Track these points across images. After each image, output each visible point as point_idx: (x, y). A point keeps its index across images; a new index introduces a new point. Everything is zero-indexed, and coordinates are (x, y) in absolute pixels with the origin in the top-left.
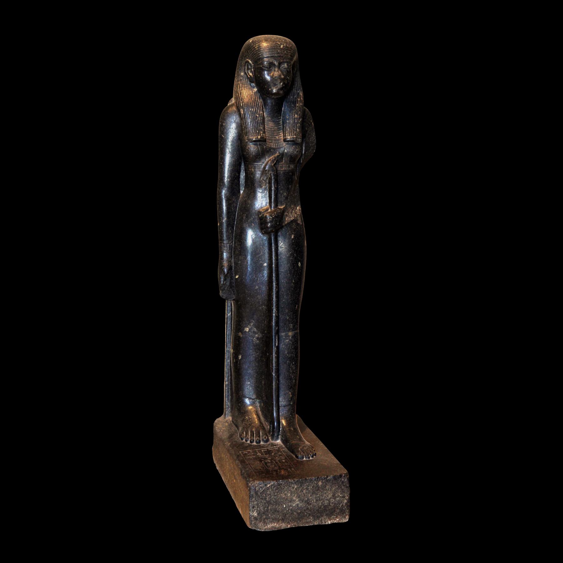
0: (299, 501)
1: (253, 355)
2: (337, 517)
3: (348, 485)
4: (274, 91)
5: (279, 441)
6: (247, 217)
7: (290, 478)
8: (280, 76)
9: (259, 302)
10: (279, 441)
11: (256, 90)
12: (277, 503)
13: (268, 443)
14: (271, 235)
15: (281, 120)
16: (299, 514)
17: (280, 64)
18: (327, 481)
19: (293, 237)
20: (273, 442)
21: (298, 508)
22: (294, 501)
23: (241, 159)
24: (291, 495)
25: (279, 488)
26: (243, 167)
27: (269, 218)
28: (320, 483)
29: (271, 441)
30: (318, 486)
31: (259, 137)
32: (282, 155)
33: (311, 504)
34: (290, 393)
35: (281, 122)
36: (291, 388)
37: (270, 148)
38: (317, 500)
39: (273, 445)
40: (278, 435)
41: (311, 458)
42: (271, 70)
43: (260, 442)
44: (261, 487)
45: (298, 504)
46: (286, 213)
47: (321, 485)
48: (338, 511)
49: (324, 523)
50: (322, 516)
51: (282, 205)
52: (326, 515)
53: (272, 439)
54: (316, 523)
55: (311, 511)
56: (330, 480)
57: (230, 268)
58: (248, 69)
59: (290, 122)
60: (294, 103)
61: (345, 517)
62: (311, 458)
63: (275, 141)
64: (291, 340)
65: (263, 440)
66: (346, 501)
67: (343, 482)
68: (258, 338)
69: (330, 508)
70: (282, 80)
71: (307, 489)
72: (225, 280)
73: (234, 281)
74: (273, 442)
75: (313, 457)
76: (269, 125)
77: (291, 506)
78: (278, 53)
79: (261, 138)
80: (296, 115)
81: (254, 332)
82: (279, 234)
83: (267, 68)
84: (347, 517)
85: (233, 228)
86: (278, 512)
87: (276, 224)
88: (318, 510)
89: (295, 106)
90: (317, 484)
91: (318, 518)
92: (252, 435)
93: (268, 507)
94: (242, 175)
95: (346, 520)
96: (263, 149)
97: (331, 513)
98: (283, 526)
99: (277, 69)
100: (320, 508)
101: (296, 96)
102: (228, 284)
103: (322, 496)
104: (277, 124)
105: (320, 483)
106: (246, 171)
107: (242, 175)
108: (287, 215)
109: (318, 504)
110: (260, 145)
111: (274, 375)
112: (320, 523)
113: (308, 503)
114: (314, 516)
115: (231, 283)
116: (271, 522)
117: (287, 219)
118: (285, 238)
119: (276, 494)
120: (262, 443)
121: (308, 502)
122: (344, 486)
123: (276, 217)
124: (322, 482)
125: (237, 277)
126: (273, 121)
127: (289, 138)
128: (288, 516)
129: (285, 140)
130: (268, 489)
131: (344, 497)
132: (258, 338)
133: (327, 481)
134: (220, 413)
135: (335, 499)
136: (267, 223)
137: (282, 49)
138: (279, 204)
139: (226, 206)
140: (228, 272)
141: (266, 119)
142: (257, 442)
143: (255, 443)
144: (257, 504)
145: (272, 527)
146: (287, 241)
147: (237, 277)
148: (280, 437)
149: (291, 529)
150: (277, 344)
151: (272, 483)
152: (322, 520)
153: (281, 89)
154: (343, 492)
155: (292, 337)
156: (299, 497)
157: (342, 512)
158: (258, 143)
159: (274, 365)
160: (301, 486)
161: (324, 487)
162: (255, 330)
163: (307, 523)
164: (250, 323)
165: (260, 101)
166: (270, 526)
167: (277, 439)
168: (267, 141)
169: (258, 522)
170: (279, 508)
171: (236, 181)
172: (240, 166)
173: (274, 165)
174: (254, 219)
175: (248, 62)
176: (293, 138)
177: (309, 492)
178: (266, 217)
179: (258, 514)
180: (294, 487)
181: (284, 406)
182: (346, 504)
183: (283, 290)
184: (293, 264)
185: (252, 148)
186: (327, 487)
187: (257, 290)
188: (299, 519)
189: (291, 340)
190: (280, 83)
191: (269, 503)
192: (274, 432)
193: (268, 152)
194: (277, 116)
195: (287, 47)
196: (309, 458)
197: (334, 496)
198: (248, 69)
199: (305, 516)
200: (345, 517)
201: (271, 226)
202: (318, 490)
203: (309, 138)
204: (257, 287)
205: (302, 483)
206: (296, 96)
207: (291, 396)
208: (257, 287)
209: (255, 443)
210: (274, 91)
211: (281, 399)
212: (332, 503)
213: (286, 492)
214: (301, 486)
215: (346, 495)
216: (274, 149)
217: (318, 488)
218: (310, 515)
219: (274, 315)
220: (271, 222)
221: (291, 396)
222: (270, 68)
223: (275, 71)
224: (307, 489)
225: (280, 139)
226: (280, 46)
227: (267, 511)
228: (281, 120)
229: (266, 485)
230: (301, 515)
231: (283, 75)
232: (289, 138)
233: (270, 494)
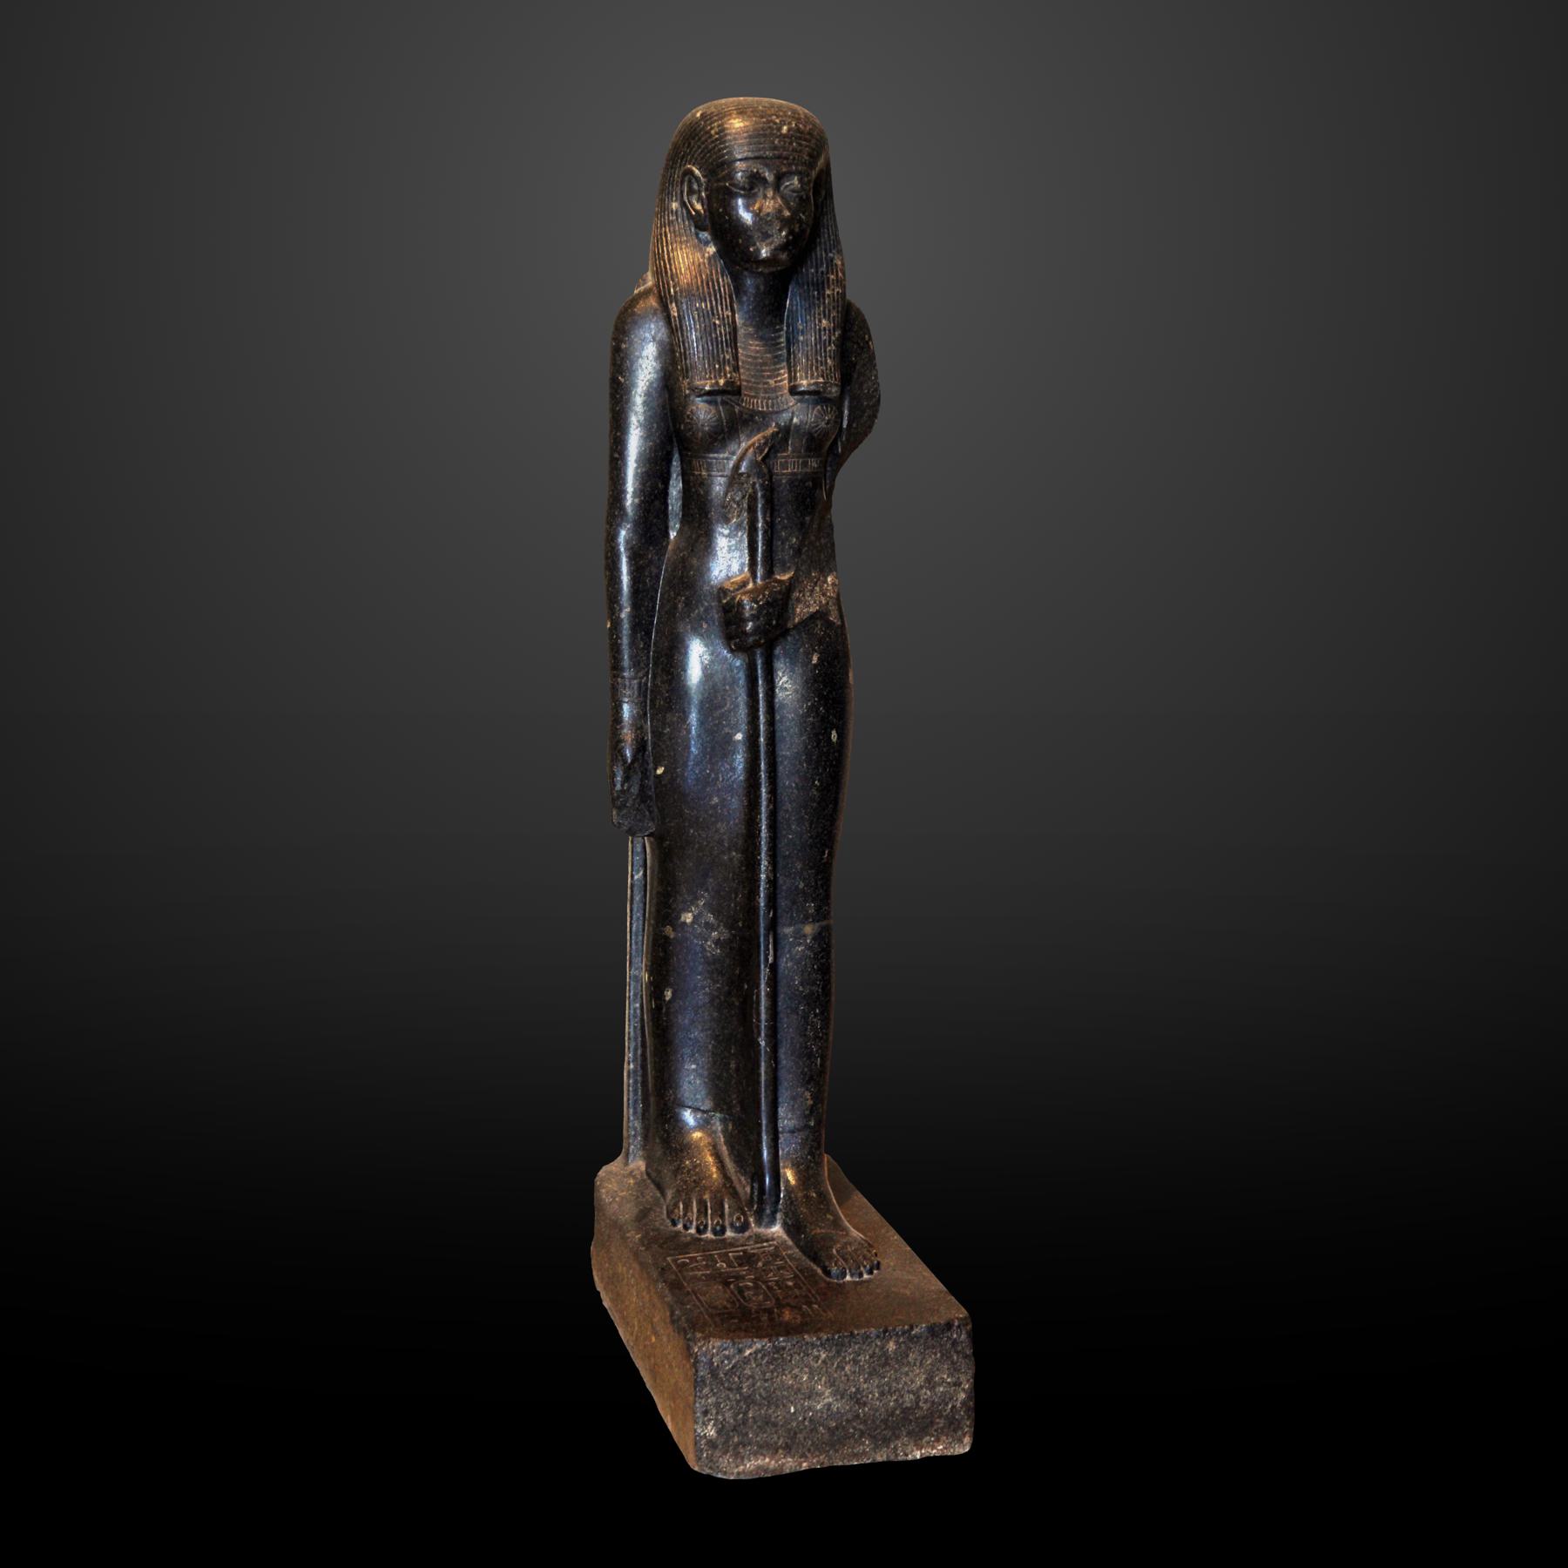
0: (833, 1394)
1: (703, 988)
2: (938, 1440)
4: (764, 253)
5: (777, 1229)
6: (688, 604)
7: (808, 1332)
8: (780, 211)
9: (721, 842)
10: (777, 1229)
11: (712, 249)
12: (771, 1400)
13: (747, 1234)
14: (754, 654)
15: (783, 333)
16: (832, 1431)
17: (779, 178)
18: (911, 1339)
19: (815, 660)
20: (762, 1230)
21: (831, 1416)
22: (820, 1395)
23: (671, 442)
24: (811, 1378)
25: (776, 1359)
26: (676, 464)
27: (748, 607)
28: (891, 1346)
29: (755, 1228)
30: (885, 1354)
31: (722, 382)
32: (786, 432)
33: (865, 1404)
34: (808, 1095)
35: (783, 340)
37: (753, 413)
38: (882, 1394)
39: (759, 1239)
40: (774, 1213)
41: (866, 1276)
42: (755, 195)
43: (723, 1231)
44: (728, 1358)
45: (829, 1405)
46: (796, 594)
47: (895, 1352)
48: (941, 1422)
49: (901, 1458)
50: (898, 1437)
51: (784, 571)
52: (909, 1434)
53: (759, 1222)
54: (881, 1457)
55: (865, 1422)
56: (918, 1337)
57: (640, 747)
58: (691, 192)
59: (807, 339)
60: (820, 286)
61: (960, 1441)
62: (866, 1276)
63: (766, 391)
64: (810, 948)
65: (732, 1225)
66: (963, 1396)
67: (955, 1343)
68: (717, 942)
69: (919, 1414)
70: (786, 223)
71: (855, 1362)
72: (627, 779)
73: (651, 782)
74: (762, 1230)
75: (870, 1272)
76: (750, 347)
77: (810, 1409)
78: (775, 148)
79: (727, 383)
80: (824, 322)
81: (707, 924)
82: (778, 651)
83: (743, 188)
84: (967, 1440)
85: (648, 634)
86: (775, 1425)
87: (769, 623)
88: (885, 1421)
89: (822, 295)
90: (882, 1348)
91: (886, 1441)
92: (703, 1211)
93: (745, 1413)
94: (675, 489)
95: (963, 1447)
96: (731, 414)
97: (921, 1428)
98: (789, 1464)
99: (770, 193)
100: (892, 1414)
101: (824, 268)
102: (635, 790)
103: (897, 1380)
104: (772, 344)
105: (891, 1346)
107: (675, 489)
108: (798, 600)
109: (887, 1404)
110: (723, 403)
111: (763, 1043)
112: (892, 1458)
113: (858, 1402)
114: (873, 1438)
115: (642, 788)
116: (755, 1454)
117: (801, 611)
119: (768, 1375)
120: (729, 1234)
121: (858, 1399)
122: (958, 1352)
123: (767, 603)
124: (897, 1343)
125: (660, 771)
126: (761, 338)
127: (804, 384)
128: (801, 1436)
129: (793, 391)
130: (747, 1361)
131: (958, 1384)
132: (717, 942)
133: (911, 1339)
134: (613, 1149)
135: (932, 1389)
136: (745, 621)
137: (785, 136)
138: (776, 570)
139: (631, 573)
140: (635, 759)
141: (741, 332)
142: (715, 1232)
143: (709, 1235)
144: (717, 1405)
145: (759, 1467)
146: (799, 670)
147: (660, 771)
148: (779, 1216)
149: (810, 1472)
151: (758, 1346)
152: (896, 1449)
153: (784, 247)
154: (954, 1369)
155: (814, 939)
156: (831, 1383)
157: (953, 1426)
158: (719, 399)
159: (763, 1016)
160: (838, 1352)
161: (902, 1357)
162: (711, 918)
163: (855, 1455)
164: (697, 898)
165: (724, 282)
166: (753, 1465)
167: (772, 1222)
168: (744, 392)
169: (718, 1453)
170: (778, 1415)
171: (657, 503)
172: (669, 462)
173: (764, 459)
174: (706, 610)
175: (692, 173)
176: (816, 384)
177: (862, 1370)
178: (740, 604)
179: (719, 1432)
180: (818, 1358)
181: (792, 1132)
182: (964, 1403)
183: (788, 806)
184: (816, 735)
185: (703, 412)
186: (911, 1357)
187: (715, 807)
188: (832, 1445)
189: (810, 948)
190: (780, 230)
191: (749, 1400)
192: (763, 1202)
193: (745, 423)
194: (772, 324)
195: (798, 130)
196: (861, 1275)
197: (929, 1380)
198: (691, 192)
199: (848, 1437)
200: (960, 1441)
201: (756, 630)
202: (886, 1364)
203: (861, 384)
204: (716, 800)
205: (840, 1346)
206: (824, 268)
207: (810, 1102)
208: (716, 800)
209: (709, 1235)
210: (764, 253)
211: (781, 1111)
212: (926, 1401)
213: (796, 1371)
214: (838, 1352)
215: (963, 1378)
216: (763, 415)
217: (885, 1360)
218: (862, 1434)
219: (763, 876)
220: (754, 618)
221: (810, 1102)
222: (751, 188)
223: (765, 197)
224: (855, 1362)
225: (781, 388)
226: (779, 129)
227: (745, 1422)
228: (783, 333)
229: (740, 1351)
230: (838, 1436)
231: (789, 209)
232: (804, 384)
233: (752, 1377)
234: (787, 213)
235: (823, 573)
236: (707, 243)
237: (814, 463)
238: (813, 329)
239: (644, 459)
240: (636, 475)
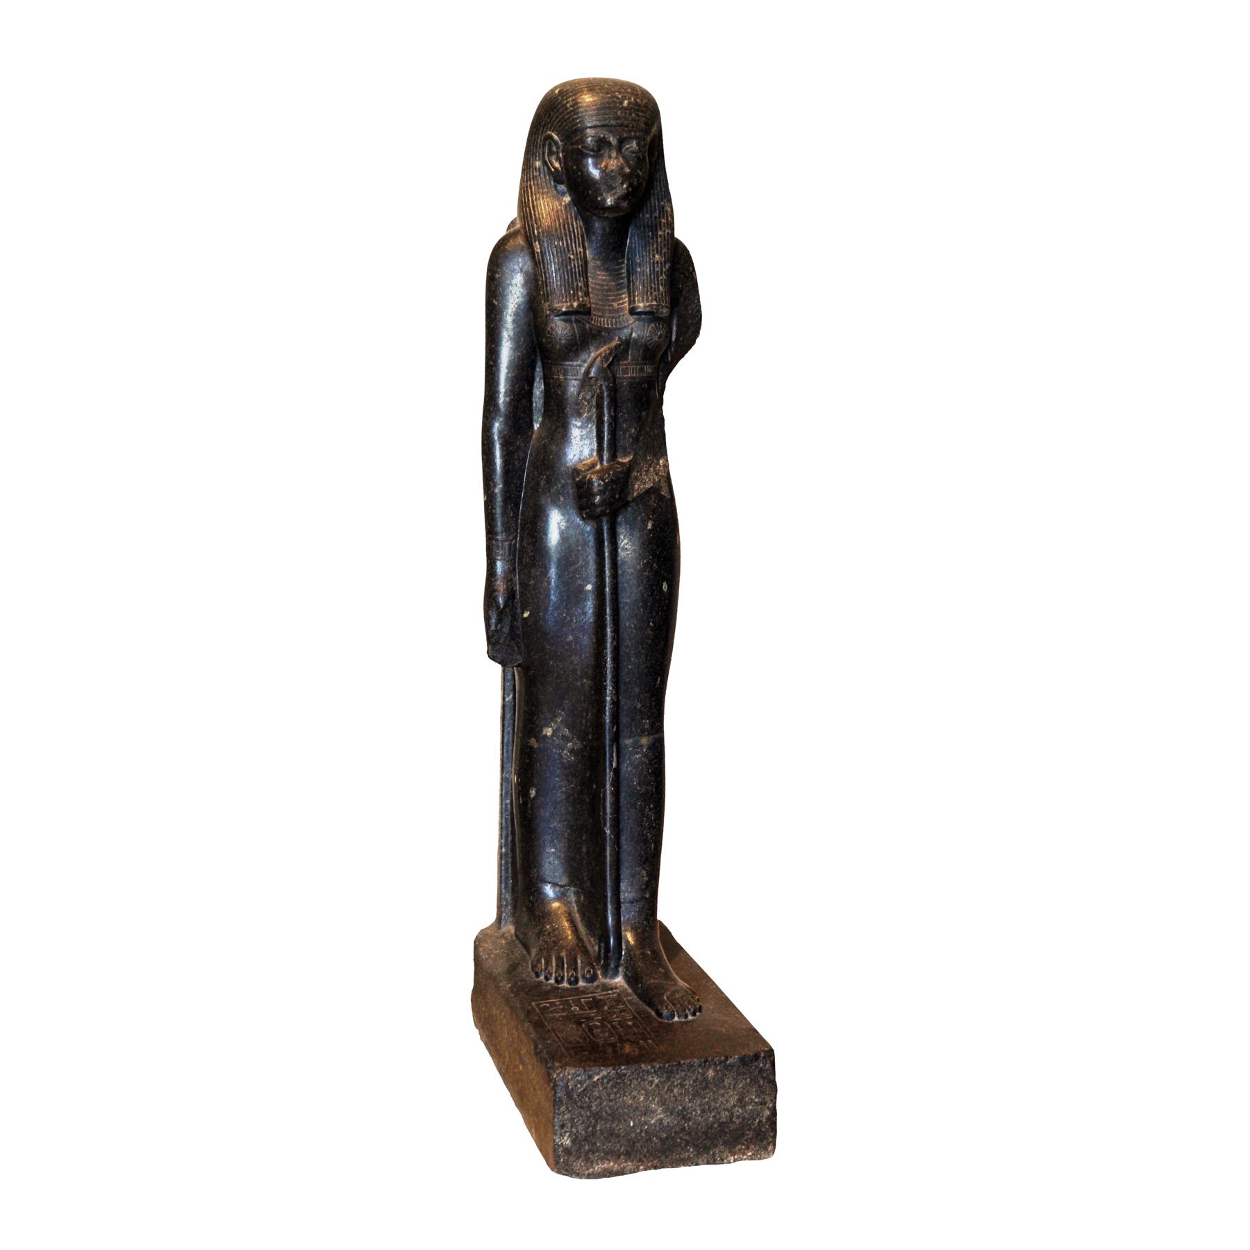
0: (664, 1111)
1: (561, 787)
2: (748, 1148)
4: (609, 202)
5: (619, 980)
6: (548, 481)
7: (644, 1062)
8: (622, 168)
9: (574, 671)
10: (619, 980)
11: (567, 199)
12: (615, 1116)
13: (595, 984)
14: (601, 522)
15: (624, 266)
16: (663, 1141)
17: (621, 142)
18: (726, 1067)
19: (650, 526)
20: (607, 981)
21: (663, 1129)
22: (654, 1112)
23: (535, 352)
24: (646, 1099)
25: (619, 1083)
26: (539, 370)
27: (597, 484)
28: (711, 1073)
29: (602, 979)
30: (706, 1079)
31: (575, 304)
32: (626, 344)
33: (689, 1119)
34: (644, 873)
35: (624, 271)
37: (600, 330)
38: (703, 1111)
39: (605, 988)
40: (617, 967)
41: (690, 1017)
42: (602, 155)
43: (576, 981)
44: (580, 1082)
45: (661, 1120)
46: (635, 474)
47: (714, 1078)
48: (750, 1134)
50: (716, 1146)
51: (625, 455)
52: (725, 1143)
53: (605, 975)
55: (689, 1134)
56: (732, 1066)
58: (551, 153)
59: (643, 270)
62: (690, 1017)
63: (610, 312)
64: (646, 756)
65: (584, 977)
68: (572, 751)
69: (732, 1127)
70: (626, 178)
71: (682, 1086)
73: (519, 624)
74: (607, 981)
75: (694, 1014)
76: (598, 277)
77: (646, 1123)
78: (618, 118)
79: (579, 306)
80: (657, 256)
81: (563, 736)
82: (620, 519)
83: (592, 150)
85: (517, 505)
86: (618, 1136)
87: (613, 497)
88: (706, 1133)
89: (655, 235)
90: (703, 1075)
92: (560, 965)
93: (594, 1127)
94: (538, 390)
96: (583, 330)
99: (614, 154)
100: (711, 1127)
101: (657, 214)
102: (506, 630)
103: (715, 1100)
104: (615, 274)
105: (711, 1073)
106: (546, 379)
107: (538, 390)
108: (636, 478)
109: (707, 1119)
110: (577, 321)
111: (608, 832)
113: (684, 1117)
114: (696, 1146)
115: (512, 628)
116: (602, 1159)
118: (632, 528)
119: (612, 1096)
120: (581, 983)
121: (684, 1115)
123: (612, 481)
124: (715, 1070)
125: (526, 615)
126: (607, 270)
127: (641, 306)
128: (638, 1145)
129: (633, 311)
130: (595, 1085)
132: (572, 751)
133: (726, 1067)
135: (743, 1107)
136: (594, 495)
137: (626, 108)
138: (619, 454)
139: (503, 457)
140: (506, 605)
141: (591, 265)
142: (570, 982)
143: (565, 985)
144: (572, 1120)
146: (637, 534)
147: (526, 615)
148: (621, 969)
150: (614, 765)
151: (605, 1073)
153: (625, 197)
155: (649, 748)
156: (663, 1103)
158: (573, 318)
159: (608, 810)
160: (668, 1078)
161: (719, 1081)
162: (567, 732)
164: (555, 716)
165: (578, 225)
167: (616, 974)
168: (593, 312)
169: (572, 1159)
170: (620, 1128)
171: (524, 401)
172: (533, 368)
173: (609, 366)
174: (563, 486)
175: (551, 138)
176: (651, 306)
177: (687, 1092)
178: (590, 482)
179: (573, 1142)
180: (652, 1082)
181: (631, 902)
183: (628, 643)
184: (651, 586)
185: (560, 329)
186: (727, 1082)
187: (570, 643)
188: (664, 1152)
189: (646, 756)
190: (622, 184)
191: (597, 1116)
193: (594, 337)
194: (615, 258)
195: (636, 104)
196: (686, 1016)
197: (741, 1100)
198: (551, 153)
199: (676, 1145)
201: (603, 502)
202: (706, 1087)
203: (687, 307)
204: (571, 638)
205: (670, 1073)
206: (657, 214)
208: (571, 638)
209: (565, 985)
210: (609, 202)
211: (623, 886)
212: (738, 1117)
213: (635, 1093)
214: (668, 1078)
216: (609, 331)
217: (706, 1085)
218: (687, 1143)
219: (608, 699)
220: (601, 492)
222: (599, 150)
223: (610, 157)
224: (682, 1086)
225: (622, 309)
226: (621, 103)
227: (594, 1134)
228: (624, 266)
229: (590, 1077)
231: (629, 166)
232: (641, 306)
233: (599, 1097)
234: (627, 170)
236: (563, 194)
237: (649, 369)
239: (513, 366)
240: (507, 378)
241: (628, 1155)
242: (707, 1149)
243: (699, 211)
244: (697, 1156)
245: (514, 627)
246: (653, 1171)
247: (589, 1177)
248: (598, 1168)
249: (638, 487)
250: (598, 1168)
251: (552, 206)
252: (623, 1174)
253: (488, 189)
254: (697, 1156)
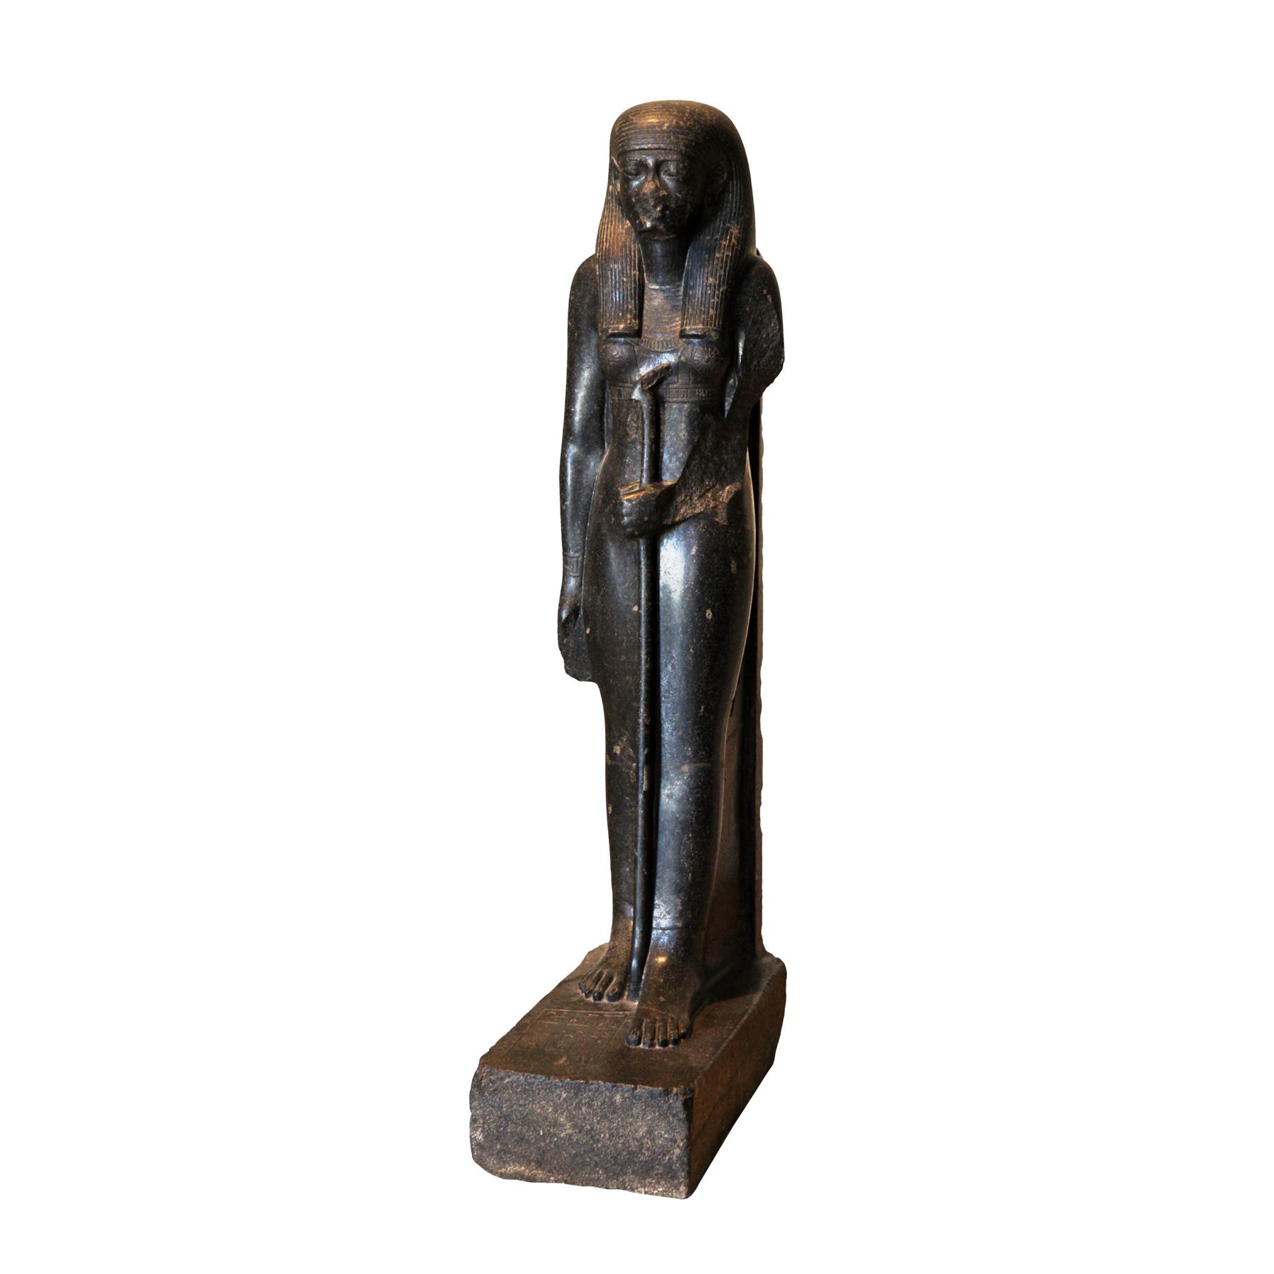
0: (574, 1127)
2: (658, 1183)
3: (682, 1116)
4: (648, 225)
8: (657, 189)
12: (525, 1121)
18: (634, 1097)
22: (562, 1125)
28: (618, 1098)
30: (613, 1103)
31: (622, 326)
34: (678, 901)
36: (678, 891)
38: (611, 1135)
41: (657, 1047)
43: (600, 996)
45: (571, 1135)
50: (625, 1174)
60: (711, 250)
62: (657, 1047)
66: (677, 1151)
69: (642, 1158)
71: (590, 1106)
73: (583, 640)
75: (665, 1043)
77: (555, 1135)
86: (528, 1142)
87: (640, 518)
89: (711, 257)
90: (611, 1098)
93: (505, 1127)
100: (620, 1154)
104: (672, 297)
108: (683, 502)
109: (615, 1146)
113: (592, 1137)
114: (606, 1170)
116: (514, 1161)
117: (684, 511)
120: (605, 1000)
122: (674, 1116)
123: (640, 503)
128: (548, 1156)
130: (506, 1088)
131: (674, 1141)
133: (634, 1097)
135: (653, 1140)
136: (623, 516)
137: (664, 132)
143: (591, 999)
144: (483, 1117)
150: (644, 788)
151: (514, 1078)
153: (662, 218)
156: (571, 1118)
164: (621, 735)
165: (635, 247)
168: (644, 334)
169: (484, 1154)
170: (531, 1135)
177: (595, 1114)
180: (560, 1096)
182: (679, 1158)
184: (691, 612)
187: (623, 662)
190: (655, 207)
191: (507, 1117)
194: (671, 282)
196: (652, 1045)
197: (650, 1132)
199: (585, 1164)
201: (631, 524)
202: (614, 1112)
203: (759, 331)
204: (623, 658)
205: (578, 1091)
208: (623, 658)
212: (648, 1149)
214: (576, 1094)
215: (678, 1137)
218: (596, 1165)
220: (629, 515)
224: (590, 1106)
228: (682, 289)
229: (502, 1079)
232: (691, 329)
235: (722, 481)
238: (706, 283)
241: (539, 1164)
242: (616, 1175)
243: (780, 234)
244: (608, 1178)
245: (590, 639)
246: (563, 1185)
247: (502, 1176)
248: (511, 1169)
249: (684, 511)
250: (511, 1169)
251: (623, 227)
252: (534, 1181)
253: (570, 215)
254: (608, 1178)
